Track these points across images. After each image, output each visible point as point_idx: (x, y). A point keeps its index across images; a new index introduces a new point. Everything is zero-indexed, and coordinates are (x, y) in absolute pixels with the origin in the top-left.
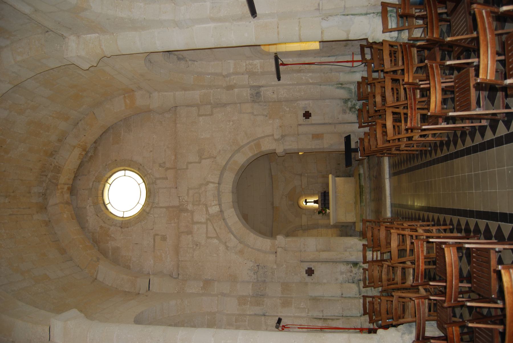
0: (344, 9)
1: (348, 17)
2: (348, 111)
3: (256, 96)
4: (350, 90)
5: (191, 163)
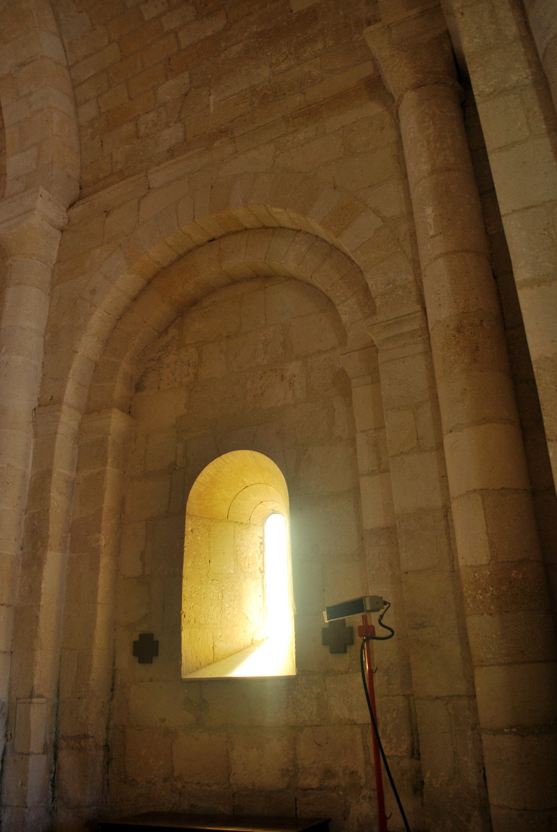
0: (22, 753)
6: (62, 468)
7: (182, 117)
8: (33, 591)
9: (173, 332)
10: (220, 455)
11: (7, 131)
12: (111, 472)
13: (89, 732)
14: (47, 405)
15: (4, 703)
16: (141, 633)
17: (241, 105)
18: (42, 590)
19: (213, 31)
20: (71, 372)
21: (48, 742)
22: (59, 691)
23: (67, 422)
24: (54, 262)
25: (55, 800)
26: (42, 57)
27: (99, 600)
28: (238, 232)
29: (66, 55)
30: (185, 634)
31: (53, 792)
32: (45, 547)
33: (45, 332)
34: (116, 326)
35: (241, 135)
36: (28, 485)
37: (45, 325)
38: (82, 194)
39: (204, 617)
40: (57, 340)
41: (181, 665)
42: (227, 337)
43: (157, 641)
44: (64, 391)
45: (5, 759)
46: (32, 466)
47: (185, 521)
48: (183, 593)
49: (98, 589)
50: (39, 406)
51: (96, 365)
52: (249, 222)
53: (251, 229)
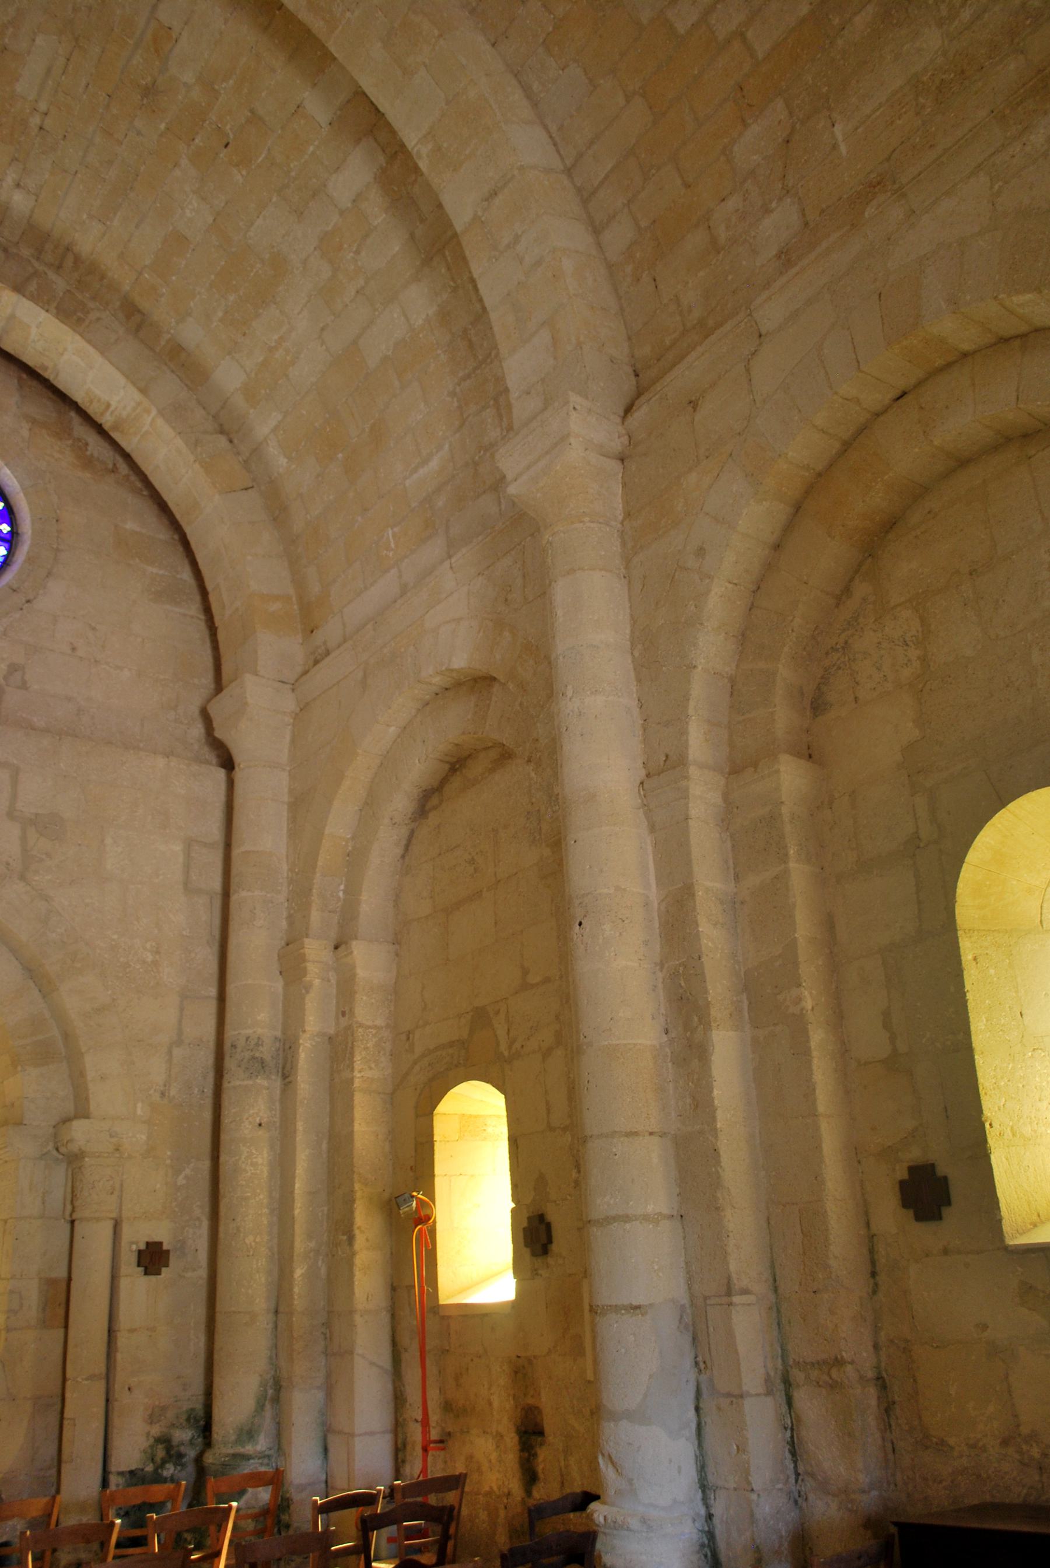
0: (729, 1395)
1: (692, 1413)
2: (156, 1430)
3: (253, 1058)
4: (248, 1434)
5: (15, 782)
6: (710, 881)
7: (790, 185)
8: (700, 1103)
9: (862, 589)
10: (1003, 805)
11: (493, 316)
12: (799, 874)
13: (844, 1354)
14: (662, 770)
15: (683, 1306)
16: (911, 1164)
17: (899, 122)
18: (716, 1102)
19: (811, 4)
20: (692, 704)
21: (772, 1374)
22: (775, 1280)
23: (703, 794)
24: (621, 518)
25: (800, 1478)
26: (521, 168)
27: (821, 1108)
28: (949, 365)
29: (558, 151)
30: (997, 1160)
31: (795, 1462)
32: (706, 1023)
33: (632, 644)
34: (752, 604)
35: (913, 179)
36: (657, 918)
37: (628, 631)
38: (640, 387)
39: (1030, 1123)
40: (655, 654)
41: (1000, 1221)
42: (971, 574)
43: (945, 1178)
44: (687, 741)
45: (701, 1405)
46: (657, 884)
47: (958, 943)
48: (981, 1080)
49: (814, 1090)
50: (648, 775)
51: (733, 681)
52: (967, 339)
53: (975, 352)
